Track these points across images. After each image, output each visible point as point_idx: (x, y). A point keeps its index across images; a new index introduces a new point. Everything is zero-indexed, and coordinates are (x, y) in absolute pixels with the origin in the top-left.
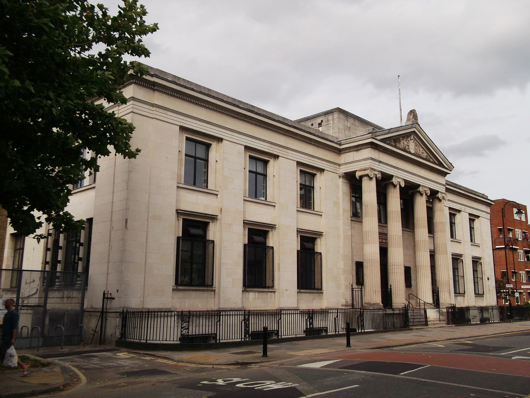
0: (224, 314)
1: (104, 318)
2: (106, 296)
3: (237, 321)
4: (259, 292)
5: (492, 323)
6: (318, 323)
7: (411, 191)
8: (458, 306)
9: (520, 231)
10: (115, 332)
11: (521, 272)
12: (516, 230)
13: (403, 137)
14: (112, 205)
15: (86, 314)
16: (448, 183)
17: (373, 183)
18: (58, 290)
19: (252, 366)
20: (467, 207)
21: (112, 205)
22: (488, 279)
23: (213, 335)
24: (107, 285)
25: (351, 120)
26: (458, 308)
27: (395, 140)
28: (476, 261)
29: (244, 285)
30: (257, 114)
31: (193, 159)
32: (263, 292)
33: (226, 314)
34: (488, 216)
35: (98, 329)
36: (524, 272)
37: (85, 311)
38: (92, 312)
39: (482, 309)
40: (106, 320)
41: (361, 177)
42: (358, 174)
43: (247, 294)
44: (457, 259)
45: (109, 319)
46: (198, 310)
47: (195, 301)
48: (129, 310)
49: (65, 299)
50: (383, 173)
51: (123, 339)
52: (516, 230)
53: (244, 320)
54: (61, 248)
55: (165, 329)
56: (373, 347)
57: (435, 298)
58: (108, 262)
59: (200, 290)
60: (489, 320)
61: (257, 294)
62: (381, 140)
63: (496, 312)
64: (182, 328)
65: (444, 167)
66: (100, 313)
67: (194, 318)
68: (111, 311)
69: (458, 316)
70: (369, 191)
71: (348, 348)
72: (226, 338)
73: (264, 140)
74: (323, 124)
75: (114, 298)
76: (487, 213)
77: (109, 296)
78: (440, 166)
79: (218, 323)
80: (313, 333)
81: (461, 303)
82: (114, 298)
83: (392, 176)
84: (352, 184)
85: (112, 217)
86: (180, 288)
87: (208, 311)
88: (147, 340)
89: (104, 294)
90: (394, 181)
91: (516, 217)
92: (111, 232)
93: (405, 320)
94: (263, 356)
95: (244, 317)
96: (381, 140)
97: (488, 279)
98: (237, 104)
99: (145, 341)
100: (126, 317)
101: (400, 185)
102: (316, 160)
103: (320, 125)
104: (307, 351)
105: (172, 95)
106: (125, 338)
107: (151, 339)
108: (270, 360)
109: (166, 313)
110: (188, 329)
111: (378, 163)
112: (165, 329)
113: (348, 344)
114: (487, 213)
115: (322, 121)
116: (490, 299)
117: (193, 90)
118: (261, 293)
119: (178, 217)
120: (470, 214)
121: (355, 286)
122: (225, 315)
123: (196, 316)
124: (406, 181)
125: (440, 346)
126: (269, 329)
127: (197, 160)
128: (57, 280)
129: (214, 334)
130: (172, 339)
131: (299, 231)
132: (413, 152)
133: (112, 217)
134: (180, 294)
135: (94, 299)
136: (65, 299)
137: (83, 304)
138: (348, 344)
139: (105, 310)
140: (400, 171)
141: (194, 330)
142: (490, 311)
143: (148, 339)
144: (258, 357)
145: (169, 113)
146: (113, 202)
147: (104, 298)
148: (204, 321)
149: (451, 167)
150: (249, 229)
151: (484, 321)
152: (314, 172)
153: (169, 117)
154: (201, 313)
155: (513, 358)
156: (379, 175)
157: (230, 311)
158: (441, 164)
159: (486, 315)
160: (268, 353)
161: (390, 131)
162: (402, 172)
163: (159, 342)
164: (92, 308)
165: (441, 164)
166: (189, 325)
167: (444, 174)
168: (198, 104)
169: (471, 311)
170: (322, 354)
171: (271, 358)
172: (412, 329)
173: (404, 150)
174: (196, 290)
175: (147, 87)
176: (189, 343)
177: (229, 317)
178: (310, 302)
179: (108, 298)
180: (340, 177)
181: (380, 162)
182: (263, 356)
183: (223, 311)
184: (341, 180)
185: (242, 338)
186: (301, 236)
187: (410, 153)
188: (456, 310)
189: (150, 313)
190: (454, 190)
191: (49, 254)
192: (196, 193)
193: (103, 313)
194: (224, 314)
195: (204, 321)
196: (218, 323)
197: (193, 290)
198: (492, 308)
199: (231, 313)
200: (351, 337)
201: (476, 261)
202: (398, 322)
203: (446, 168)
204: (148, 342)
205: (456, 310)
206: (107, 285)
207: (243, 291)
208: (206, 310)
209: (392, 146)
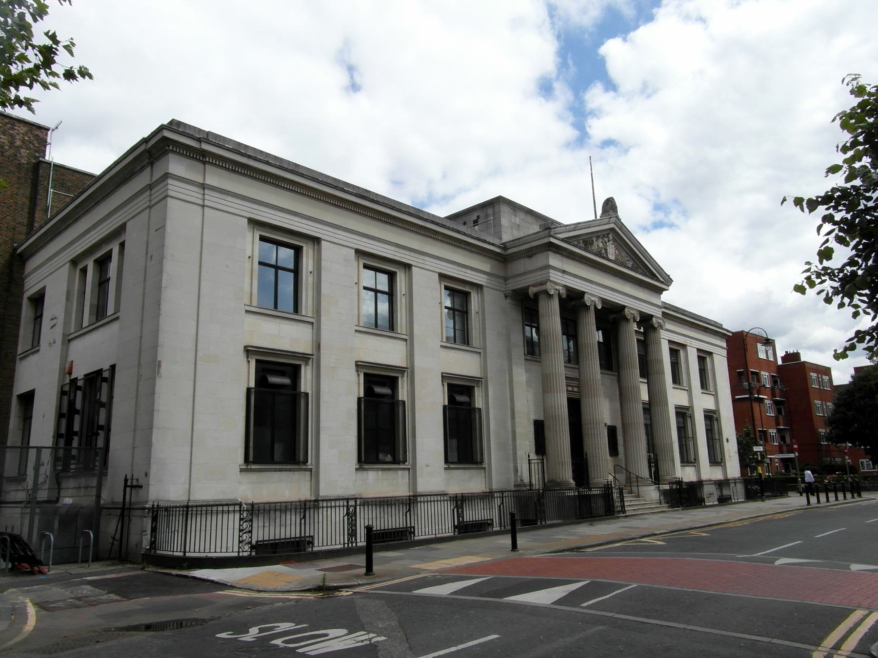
0: (325, 505)
1: (126, 519)
2: (129, 483)
3: (338, 515)
4: (383, 470)
5: (735, 503)
6: (471, 514)
7: (613, 316)
8: (685, 480)
9: (767, 374)
10: (142, 541)
11: (770, 431)
12: (762, 373)
13: (598, 237)
14: (141, 341)
15: (104, 512)
16: (666, 306)
17: (555, 304)
18: (73, 477)
19: (341, 594)
20: (694, 342)
21: (141, 341)
22: (728, 441)
23: (308, 539)
24: (132, 465)
25: (521, 215)
26: (686, 483)
27: (586, 241)
28: (711, 417)
29: (359, 460)
30: (372, 201)
31: (273, 270)
32: (389, 469)
33: (329, 505)
34: (724, 353)
35: (118, 536)
36: (775, 431)
37: (103, 508)
38: (111, 508)
39: (721, 484)
40: (130, 520)
41: (536, 295)
42: (532, 291)
43: (365, 473)
44: (684, 414)
45: (134, 520)
46: (265, 501)
47: (281, 486)
48: (162, 504)
49: (83, 490)
50: (569, 289)
51: (153, 551)
52: (762, 373)
53: (348, 514)
54: (77, 412)
55: (325, 523)
56: (553, 549)
57: (653, 469)
58: (135, 430)
59: (286, 470)
60: (730, 498)
61: (380, 473)
62: (563, 240)
63: (740, 488)
64: (240, 531)
65: (658, 280)
66: (120, 511)
67: (278, 513)
68: (136, 506)
69: (686, 496)
70: (552, 317)
71: (514, 553)
72: (329, 543)
73: (388, 242)
74: (480, 221)
75: (141, 487)
76: (722, 347)
77: (135, 483)
78: (652, 279)
79: (303, 521)
80: (467, 530)
81: (687, 475)
82: (141, 487)
83: (582, 294)
84: (525, 308)
85: (139, 360)
86: (253, 467)
87: (300, 501)
88: (185, 552)
89: (126, 480)
90: (587, 299)
91: (762, 356)
92: (138, 382)
93: (607, 506)
94: (366, 574)
95: (348, 509)
96: (563, 240)
97: (728, 441)
98: (341, 186)
99: (181, 554)
100: (157, 516)
101: (595, 306)
102: (469, 272)
103: (476, 222)
104: (443, 561)
105: (234, 171)
106: (155, 549)
107: (192, 550)
108: (378, 580)
109: (210, 508)
110: (250, 532)
111: (561, 274)
112: (325, 523)
113: (514, 546)
114: (722, 347)
115: (478, 217)
116: (733, 469)
117: (267, 163)
118: (386, 472)
119: (248, 358)
120: (699, 350)
121: (533, 456)
122: (327, 507)
123: (281, 510)
124: (604, 301)
125: (659, 543)
126: (374, 529)
127: (280, 271)
128: (72, 462)
129: (310, 536)
130: (218, 550)
131: (444, 377)
132: (612, 257)
133: (139, 360)
134: (253, 477)
135: (113, 492)
136: (83, 490)
137: (99, 496)
138: (514, 546)
139: (127, 506)
140: (593, 286)
141: (293, 532)
142: (732, 485)
143: (187, 550)
144: (358, 576)
145: (230, 199)
146: (141, 337)
147: (126, 486)
148: (293, 517)
149: (668, 281)
150: (365, 374)
151: (724, 501)
152: (467, 289)
153: (229, 204)
154: (267, 506)
155: (777, 563)
156: (563, 292)
157: (335, 500)
158: (653, 276)
159: (726, 492)
160: (375, 568)
161: (577, 226)
162: (599, 288)
163: (204, 555)
164: (113, 503)
165: (653, 276)
166: (251, 526)
167: (659, 291)
168: (277, 186)
169: (705, 487)
170: (459, 569)
171: (378, 576)
172: (619, 517)
173: (599, 254)
174: (280, 470)
175: (189, 157)
176: (266, 553)
177: (333, 509)
178: (467, 482)
179: (132, 487)
180: (506, 297)
181: (564, 272)
182: (366, 574)
183: (421, 496)
184: (509, 301)
185: (344, 544)
186: (449, 385)
187: (610, 260)
188: (684, 487)
189: (190, 509)
190: (675, 315)
191: (64, 422)
192: (278, 321)
193: (125, 511)
194: (325, 505)
195: (293, 517)
196: (303, 521)
197: (275, 470)
198: (735, 481)
199: (337, 504)
200: (518, 535)
201: (711, 417)
202: (599, 506)
203: (662, 282)
204: (187, 554)
205: (684, 487)
206: (132, 465)
207: (356, 469)
208: (297, 500)
209: (580, 248)
